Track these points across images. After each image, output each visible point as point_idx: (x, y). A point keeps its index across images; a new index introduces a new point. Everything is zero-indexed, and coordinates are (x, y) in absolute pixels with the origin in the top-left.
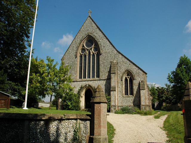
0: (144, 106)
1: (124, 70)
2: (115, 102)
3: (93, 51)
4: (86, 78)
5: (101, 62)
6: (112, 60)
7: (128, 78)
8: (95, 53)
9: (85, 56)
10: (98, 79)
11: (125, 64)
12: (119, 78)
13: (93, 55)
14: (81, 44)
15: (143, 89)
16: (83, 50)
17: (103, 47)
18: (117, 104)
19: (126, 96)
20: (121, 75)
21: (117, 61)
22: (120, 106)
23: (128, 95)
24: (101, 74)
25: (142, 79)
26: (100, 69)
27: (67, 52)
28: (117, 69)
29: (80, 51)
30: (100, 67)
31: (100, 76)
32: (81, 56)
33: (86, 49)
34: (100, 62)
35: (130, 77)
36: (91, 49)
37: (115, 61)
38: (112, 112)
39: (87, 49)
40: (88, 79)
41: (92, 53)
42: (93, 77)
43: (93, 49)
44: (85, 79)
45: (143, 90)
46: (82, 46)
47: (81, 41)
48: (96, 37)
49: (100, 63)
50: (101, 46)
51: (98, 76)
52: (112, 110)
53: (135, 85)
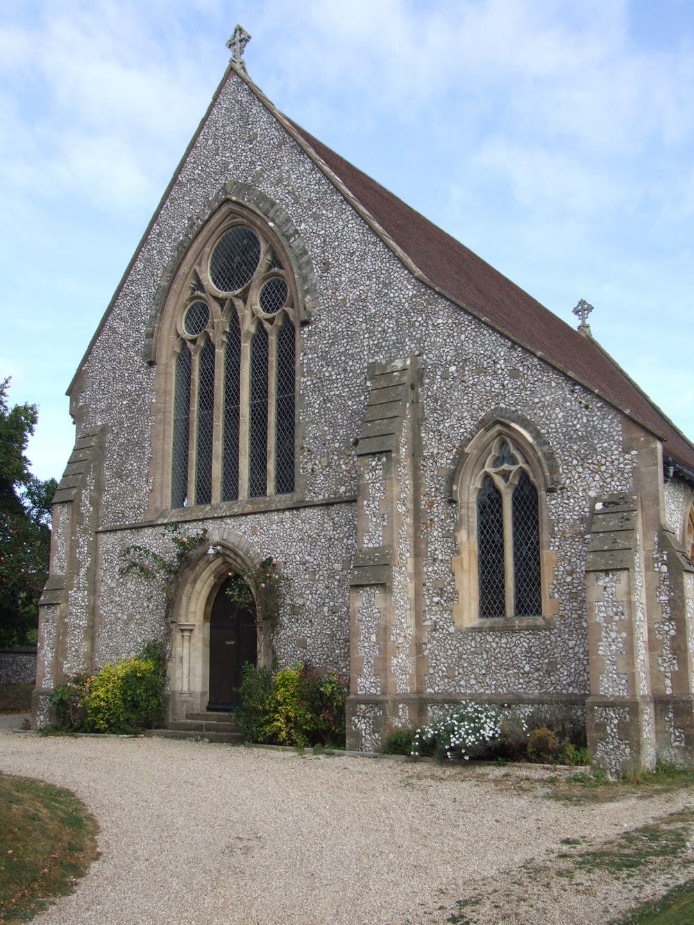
0: (612, 705)
1: (469, 424)
2: (382, 668)
3: (258, 307)
4: (265, 493)
5: (303, 381)
6: (380, 358)
7: (505, 475)
8: (271, 321)
9: (208, 353)
10: (286, 499)
11: (481, 370)
12: (428, 483)
13: (260, 339)
14: (184, 269)
15: (611, 564)
16: (198, 316)
17: (317, 272)
18: (644, 688)
19: (488, 622)
20: (446, 461)
21: (414, 363)
22: (434, 701)
23: (501, 611)
24: (303, 465)
25: (615, 486)
26: (298, 432)
27: (103, 337)
28: (418, 422)
29: (177, 323)
30: (300, 416)
31: (299, 481)
32: (184, 359)
33: (216, 298)
34: (297, 378)
35: (523, 475)
36: (244, 297)
37: (399, 364)
38: (358, 746)
39: (221, 301)
40: (224, 508)
41: (248, 327)
42: (204, 496)
43: (255, 297)
44: (261, 502)
45: (607, 572)
46: (191, 282)
47: (183, 249)
48: (273, 204)
49: (299, 390)
50: (309, 263)
51: (286, 483)
52: (358, 735)
53: (553, 534)
